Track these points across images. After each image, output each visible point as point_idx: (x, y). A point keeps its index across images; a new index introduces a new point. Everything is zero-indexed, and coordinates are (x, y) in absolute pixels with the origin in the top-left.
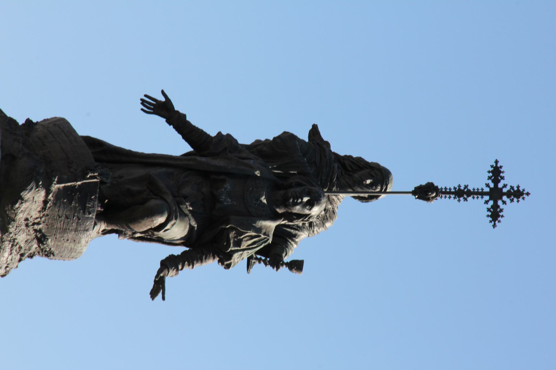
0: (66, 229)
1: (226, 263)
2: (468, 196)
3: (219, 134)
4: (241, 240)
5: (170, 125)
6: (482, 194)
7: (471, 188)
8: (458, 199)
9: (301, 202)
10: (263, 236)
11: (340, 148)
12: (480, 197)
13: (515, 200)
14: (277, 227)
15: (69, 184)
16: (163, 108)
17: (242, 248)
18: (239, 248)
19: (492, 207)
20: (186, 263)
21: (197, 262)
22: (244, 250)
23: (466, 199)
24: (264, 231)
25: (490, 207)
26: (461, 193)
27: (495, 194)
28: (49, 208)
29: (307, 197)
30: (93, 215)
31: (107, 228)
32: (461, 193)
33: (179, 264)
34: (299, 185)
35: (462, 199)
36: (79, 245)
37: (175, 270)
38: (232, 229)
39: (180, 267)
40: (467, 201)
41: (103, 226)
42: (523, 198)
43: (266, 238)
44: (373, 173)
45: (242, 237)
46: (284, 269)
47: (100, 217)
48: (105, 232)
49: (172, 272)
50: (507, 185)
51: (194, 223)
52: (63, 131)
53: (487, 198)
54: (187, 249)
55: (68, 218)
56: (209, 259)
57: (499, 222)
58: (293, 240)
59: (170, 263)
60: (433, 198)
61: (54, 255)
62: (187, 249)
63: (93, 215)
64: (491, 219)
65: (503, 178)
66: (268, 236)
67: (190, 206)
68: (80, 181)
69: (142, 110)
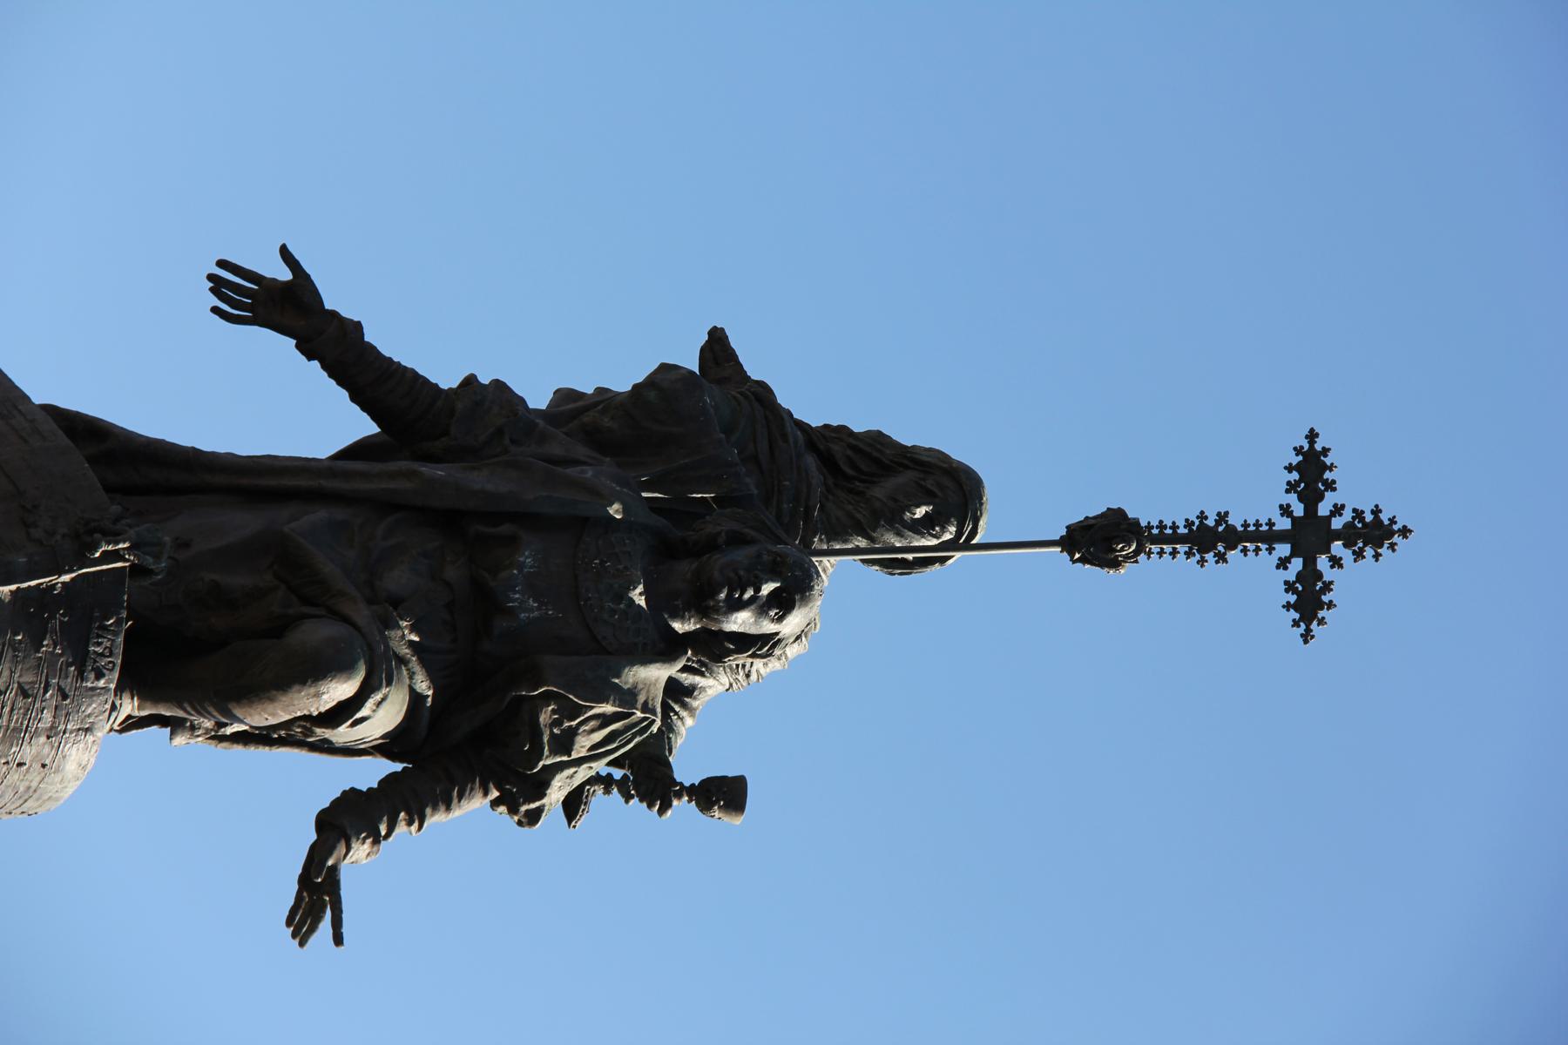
0: (17, 730)
1: (523, 808)
3: (470, 381)
4: (572, 734)
5: (310, 358)
6: (1269, 537)
7: (1236, 521)
8: (1198, 557)
9: (753, 599)
10: (639, 714)
11: (810, 402)
12: (1263, 546)
13: (1369, 552)
14: (671, 680)
15: (33, 583)
16: (281, 304)
17: (574, 755)
18: (565, 758)
19: (1300, 577)
20: (402, 815)
21: (435, 809)
23: (1221, 558)
24: (641, 699)
25: (1292, 578)
26: (1209, 538)
27: (1309, 536)
29: (773, 581)
30: (108, 682)
31: (136, 713)
32: (1209, 538)
33: (380, 820)
34: (737, 540)
35: (1209, 556)
36: (58, 778)
37: (369, 841)
38: (547, 697)
39: (383, 830)
40: (1225, 561)
41: (129, 707)
42: (1392, 547)
43: (645, 719)
44: (929, 484)
45: (574, 723)
47: (131, 682)
49: (361, 851)
50: (1343, 506)
51: (423, 686)
53: (1283, 549)
54: (398, 767)
55: (25, 695)
56: (471, 797)
57: (1321, 622)
58: (684, 706)
59: (347, 819)
60: (1127, 557)
62: (398, 767)
63: (108, 682)
64: (1297, 616)
65: (1330, 485)
66: (654, 714)
67: (413, 629)
68: (71, 571)
69: (215, 310)
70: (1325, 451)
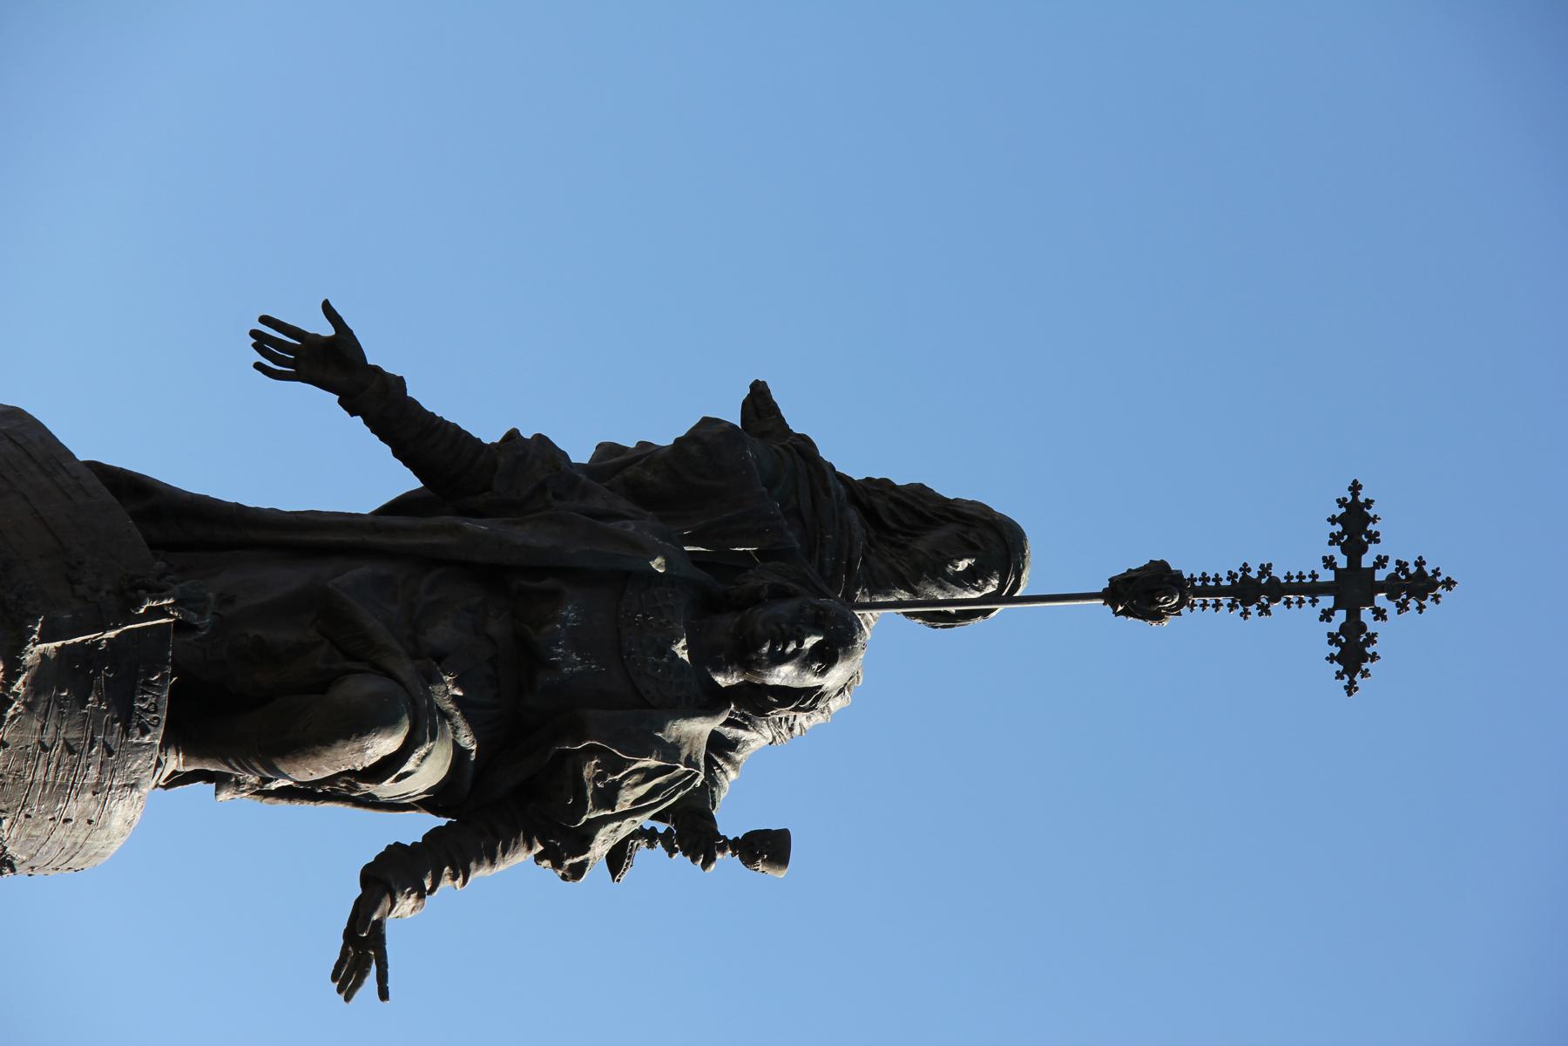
1: (568, 862)
2: (1274, 599)
3: (513, 435)
4: (615, 788)
6: (1313, 589)
7: (1279, 573)
8: (1241, 609)
10: (682, 768)
11: (853, 453)
12: (1307, 599)
14: (714, 734)
16: (324, 359)
17: (618, 809)
18: (609, 812)
21: (479, 863)
22: (623, 816)
23: (1264, 610)
24: (685, 752)
26: (1252, 590)
27: (1352, 588)
28: (13, 718)
29: (816, 634)
30: (153, 738)
31: (181, 769)
32: (1252, 590)
33: (425, 875)
34: (780, 593)
35: (1253, 608)
36: (104, 834)
37: (414, 896)
38: (591, 752)
40: (1268, 613)
41: (174, 763)
42: (1436, 599)
43: (688, 773)
44: (972, 536)
46: (726, 861)
48: (176, 780)
49: (406, 905)
50: (1386, 558)
51: (467, 741)
52: (29, 455)
53: (1327, 602)
55: (71, 751)
57: (1365, 674)
58: (728, 759)
59: (392, 874)
60: (1170, 610)
61: (13, 870)
63: (153, 738)
64: (1341, 668)
65: (1374, 538)
67: (456, 684)
68: (111, 629)
69: (258, 366)
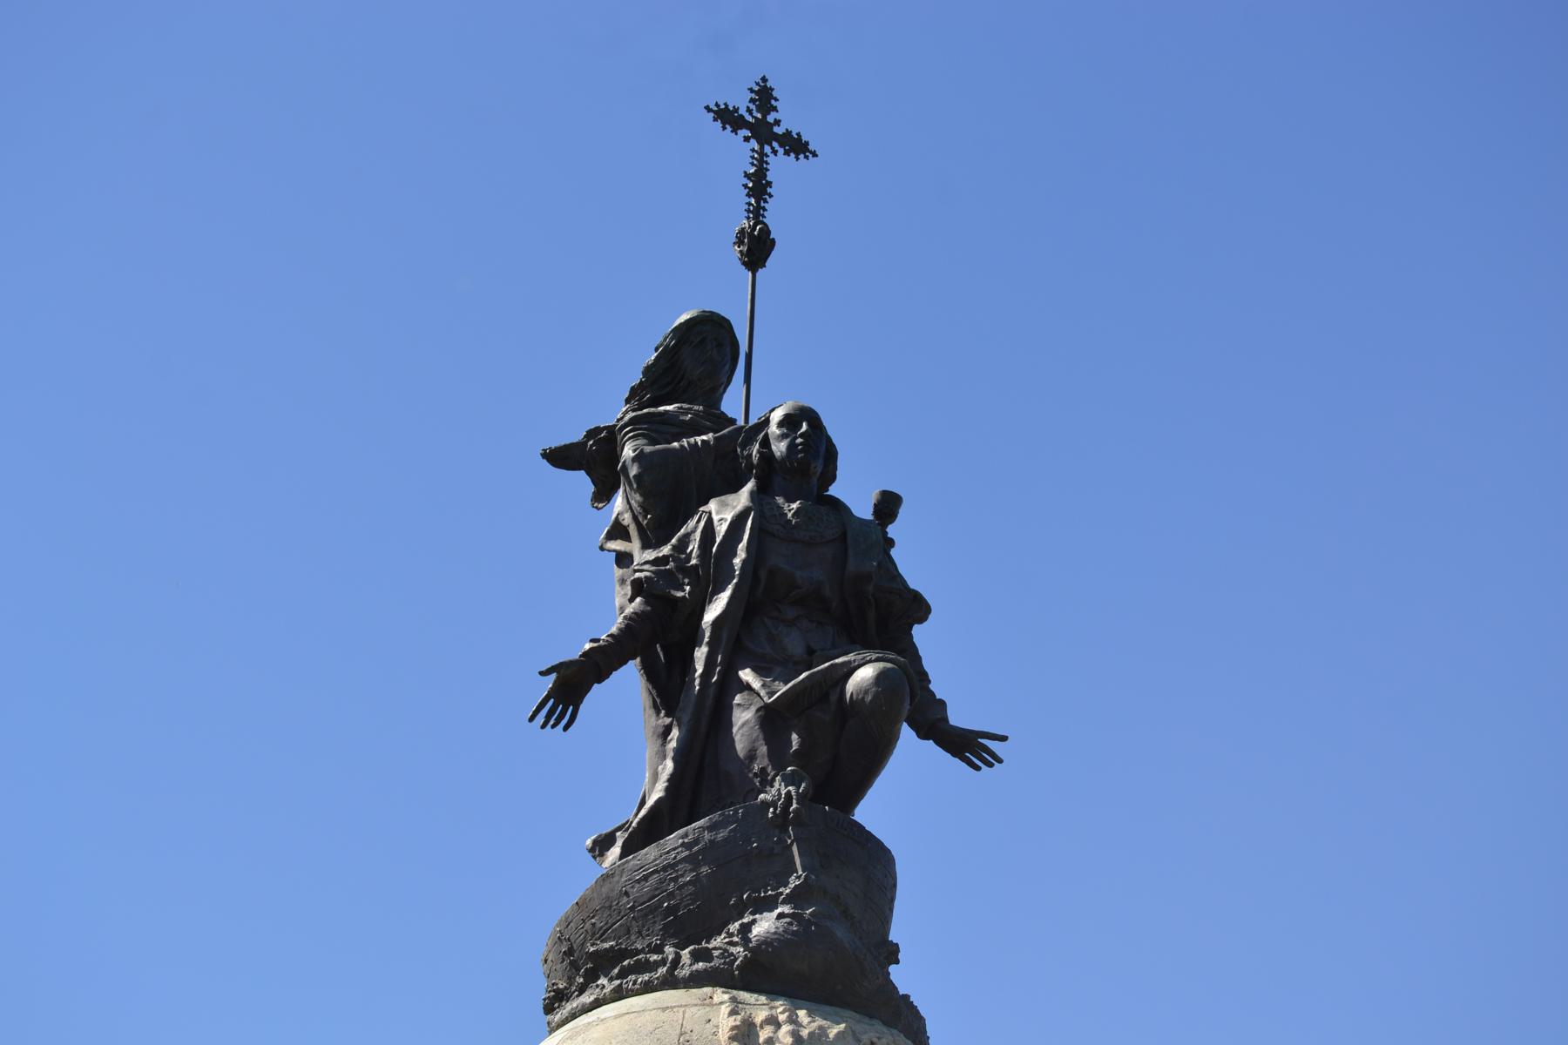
16: (571, 685)
26: (759, 187)
32: (759, 187)
69: (566, 728)
70: (717, 105)
